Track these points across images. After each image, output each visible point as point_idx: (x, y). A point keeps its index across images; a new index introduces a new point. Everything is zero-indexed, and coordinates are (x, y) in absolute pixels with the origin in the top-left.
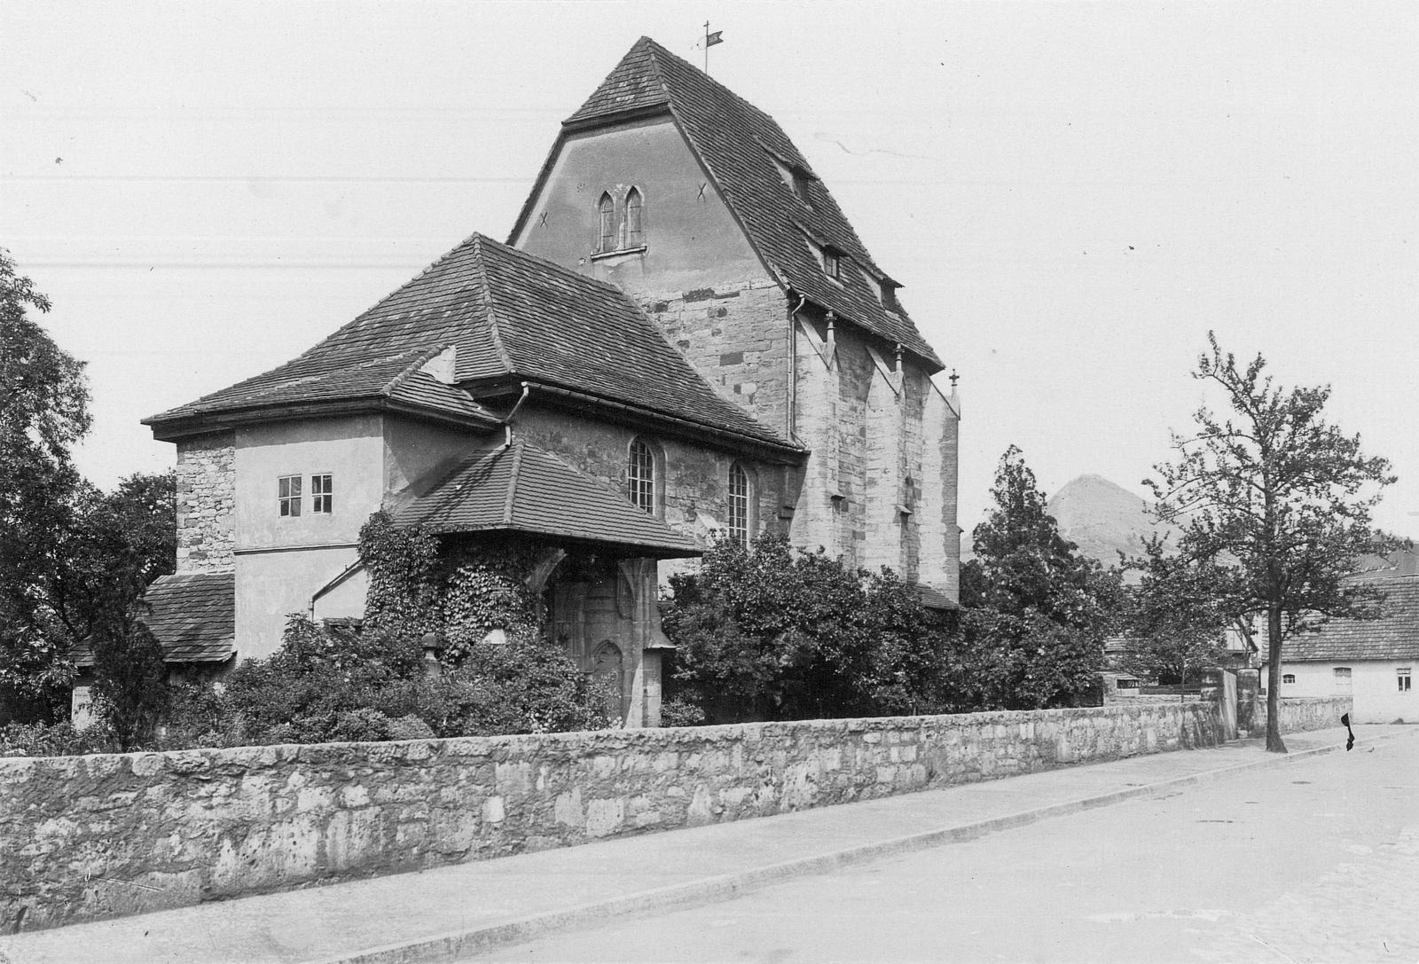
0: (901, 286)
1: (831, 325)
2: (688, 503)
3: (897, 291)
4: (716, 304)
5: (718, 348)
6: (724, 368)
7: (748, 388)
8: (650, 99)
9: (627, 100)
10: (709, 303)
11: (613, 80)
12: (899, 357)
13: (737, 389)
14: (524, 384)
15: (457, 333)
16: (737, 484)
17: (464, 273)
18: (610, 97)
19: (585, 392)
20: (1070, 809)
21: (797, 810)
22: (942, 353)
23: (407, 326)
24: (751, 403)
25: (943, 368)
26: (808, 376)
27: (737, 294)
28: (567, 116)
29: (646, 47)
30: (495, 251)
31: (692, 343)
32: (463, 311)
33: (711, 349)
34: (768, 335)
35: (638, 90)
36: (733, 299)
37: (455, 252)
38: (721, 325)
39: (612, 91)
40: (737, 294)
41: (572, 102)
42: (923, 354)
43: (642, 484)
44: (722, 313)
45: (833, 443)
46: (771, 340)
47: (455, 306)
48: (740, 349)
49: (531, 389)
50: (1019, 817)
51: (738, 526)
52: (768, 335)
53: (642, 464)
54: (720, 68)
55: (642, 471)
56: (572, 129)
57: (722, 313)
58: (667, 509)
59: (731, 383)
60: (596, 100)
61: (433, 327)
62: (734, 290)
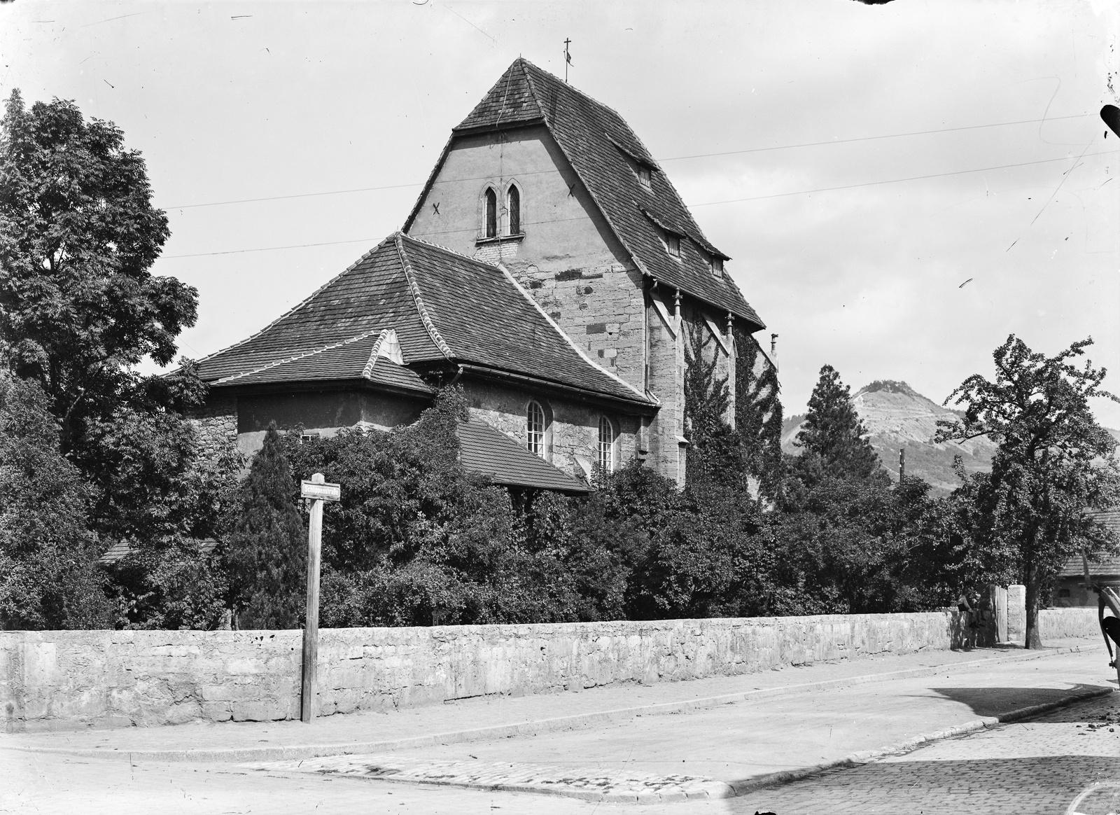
0: (727, 259)
1: (678, 302)
2: (569, 450)
3: (725, 262)
4: (583, 283)
5: (585, 320)
6: (590, 336)
7: (610, 353)
8: (526, 115)
9: (505, 112)
10: (576, 282)
11: (495, 95)
12: (730, 323)
13: (601, 353)
14: (460, 365)
15: (394, 319)
16: (604, 437)
17: (392, 267)
18: (493, 109)
19: (497, 368)
20: (158, 757)
21: (10, 710)
22: (763, 316)
23: (350, 310)
24: (612, 365)
25: (764, 328)
26: (659, 343)
27: (600, 276)
28: (456, 122)
29: (520, 63)
30: (413, 246)
31: (562, 315)
32: (395, 300)
33: (578, 321)
34: (627, 310)
35: (516, 106)
36: (598, 280)
37: (380, 247)
38: (588, 300)
39: (494, 104)
40: (600, 276)
41: (460, 114)
42: (747, 317)
43: (536, 435)
44: (588, 291)
45: (679, 399)
46: (630, 315)
47: (388, 295)
48: (602, 321)
49: (465, 369)
50: (253, 753)
51: (536, 430)
52: (627, 310)
53: (536, 420)
54: (579, 79)
55: (536, 426)
56: (463, 137)
57: (588, 291)
58: (554, 455)
59: (595, 349)
60: (482, 110)
61: (372, 313)
62: (598, 272)
